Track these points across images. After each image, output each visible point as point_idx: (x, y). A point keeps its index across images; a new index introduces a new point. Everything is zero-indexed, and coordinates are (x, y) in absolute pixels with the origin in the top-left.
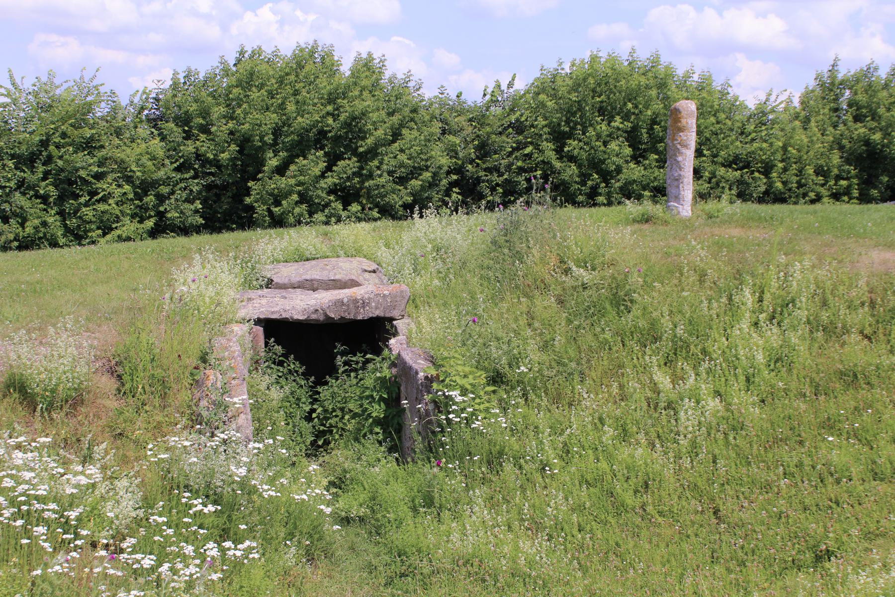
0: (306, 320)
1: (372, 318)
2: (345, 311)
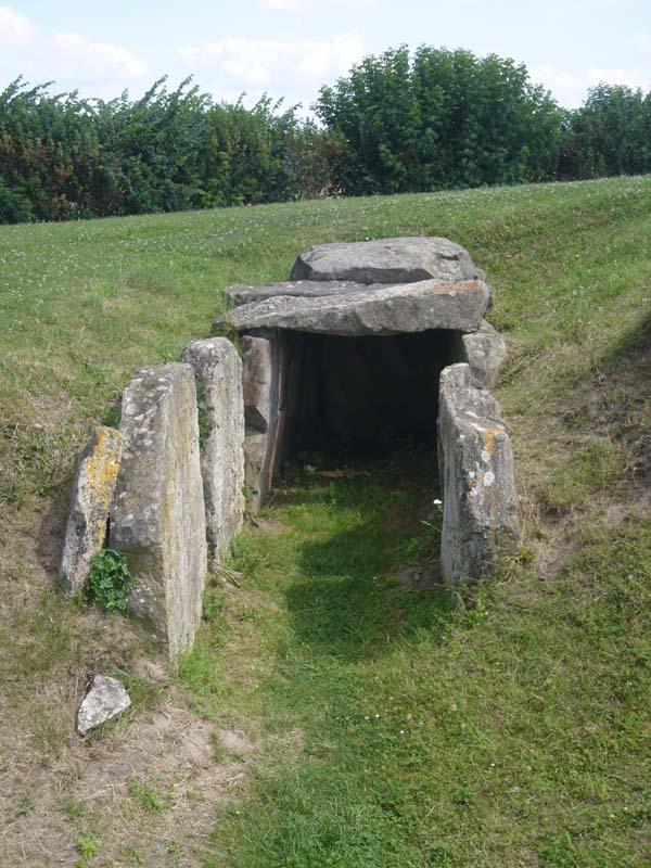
1: (429, 332)
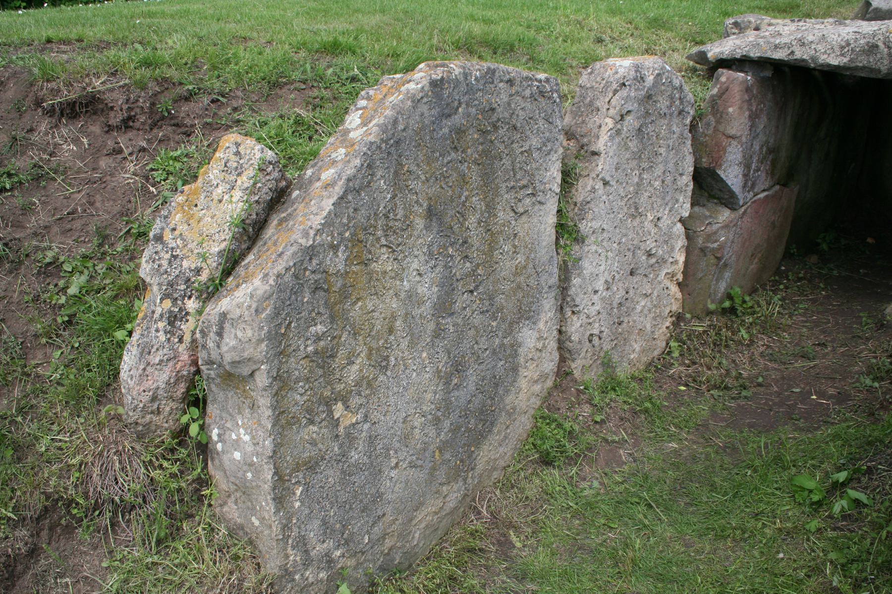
0: (845, 68)
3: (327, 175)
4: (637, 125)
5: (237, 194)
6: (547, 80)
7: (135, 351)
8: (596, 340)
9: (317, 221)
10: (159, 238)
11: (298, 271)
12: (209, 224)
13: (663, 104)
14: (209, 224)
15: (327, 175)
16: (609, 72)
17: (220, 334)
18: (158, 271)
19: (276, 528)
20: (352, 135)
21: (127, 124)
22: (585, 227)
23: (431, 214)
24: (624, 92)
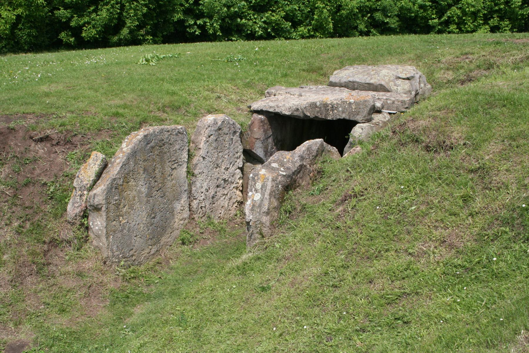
1: (339, 120)
2: (318, 112)
3: (118, 161)
4: (215, 138)
5: (97, 166)
6: (181, 128)
7: (71, 204)
8: (203, 209)
9: (116, 172)
10: (78, 177)
11: (112, 184)
12: (90, 173)
13: (226, 130)
14: (90, 173)
15: (118, 161)
16: (206, 122)
17: (94, 198)
18: (78, 184)
19: (106, 245)
20: (124, 150)
21: (58, 144)
22: (196, 172)
23: (145, 170)
24: (209, 129)
